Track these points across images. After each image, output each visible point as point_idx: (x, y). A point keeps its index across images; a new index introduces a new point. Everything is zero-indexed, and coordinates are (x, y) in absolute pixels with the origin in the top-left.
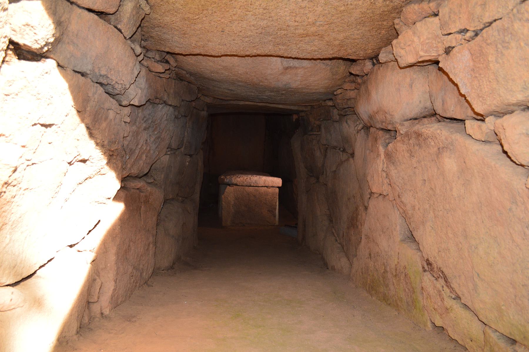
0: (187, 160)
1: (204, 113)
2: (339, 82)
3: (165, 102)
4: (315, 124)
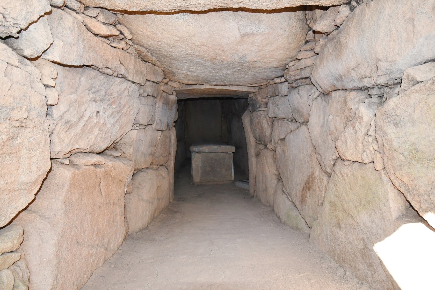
0: (158, 135)
1: (173, 98)
2: (293, 53)
3: (123, 77)
4: (262, 101)
